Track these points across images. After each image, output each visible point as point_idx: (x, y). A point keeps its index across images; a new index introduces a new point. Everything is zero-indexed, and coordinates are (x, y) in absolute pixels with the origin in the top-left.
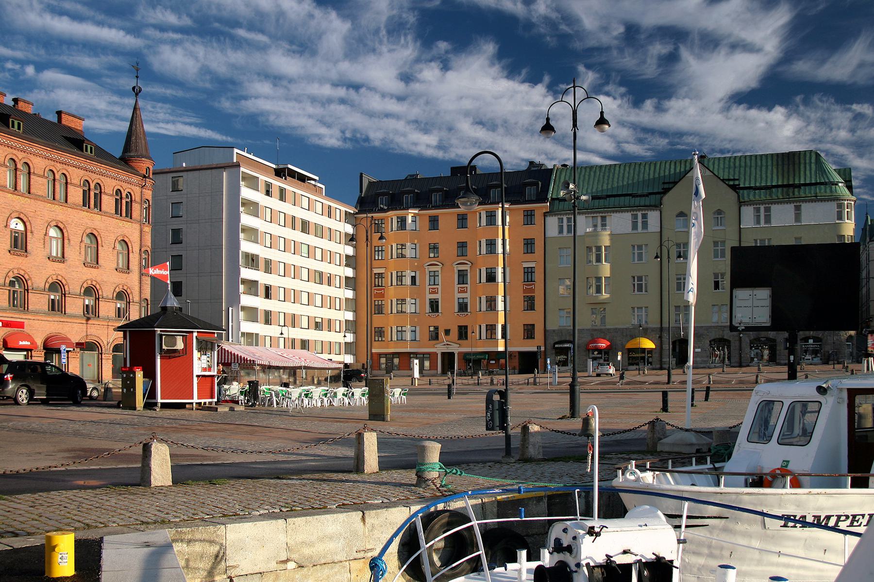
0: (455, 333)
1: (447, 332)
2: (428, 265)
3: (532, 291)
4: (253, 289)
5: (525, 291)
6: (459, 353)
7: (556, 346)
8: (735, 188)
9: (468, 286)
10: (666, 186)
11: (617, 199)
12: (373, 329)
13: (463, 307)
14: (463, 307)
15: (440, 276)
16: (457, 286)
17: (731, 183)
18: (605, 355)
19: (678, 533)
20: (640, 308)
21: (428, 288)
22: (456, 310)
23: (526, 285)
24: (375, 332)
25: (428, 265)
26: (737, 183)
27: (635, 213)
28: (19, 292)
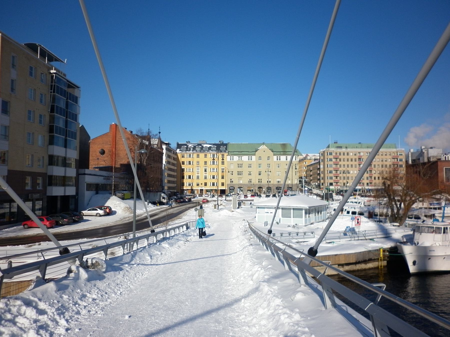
0: (203, 184)
1: (202, 184)
5: (222, 174)
6: (205, 189)
8: (272, 151)
9: (207, 172)
10: (256, 150)
13: (206, 178)
14: (206, 178)
16: (204, 172)
17: (272, 150)
20: (240, 172)
26: (273, 150)
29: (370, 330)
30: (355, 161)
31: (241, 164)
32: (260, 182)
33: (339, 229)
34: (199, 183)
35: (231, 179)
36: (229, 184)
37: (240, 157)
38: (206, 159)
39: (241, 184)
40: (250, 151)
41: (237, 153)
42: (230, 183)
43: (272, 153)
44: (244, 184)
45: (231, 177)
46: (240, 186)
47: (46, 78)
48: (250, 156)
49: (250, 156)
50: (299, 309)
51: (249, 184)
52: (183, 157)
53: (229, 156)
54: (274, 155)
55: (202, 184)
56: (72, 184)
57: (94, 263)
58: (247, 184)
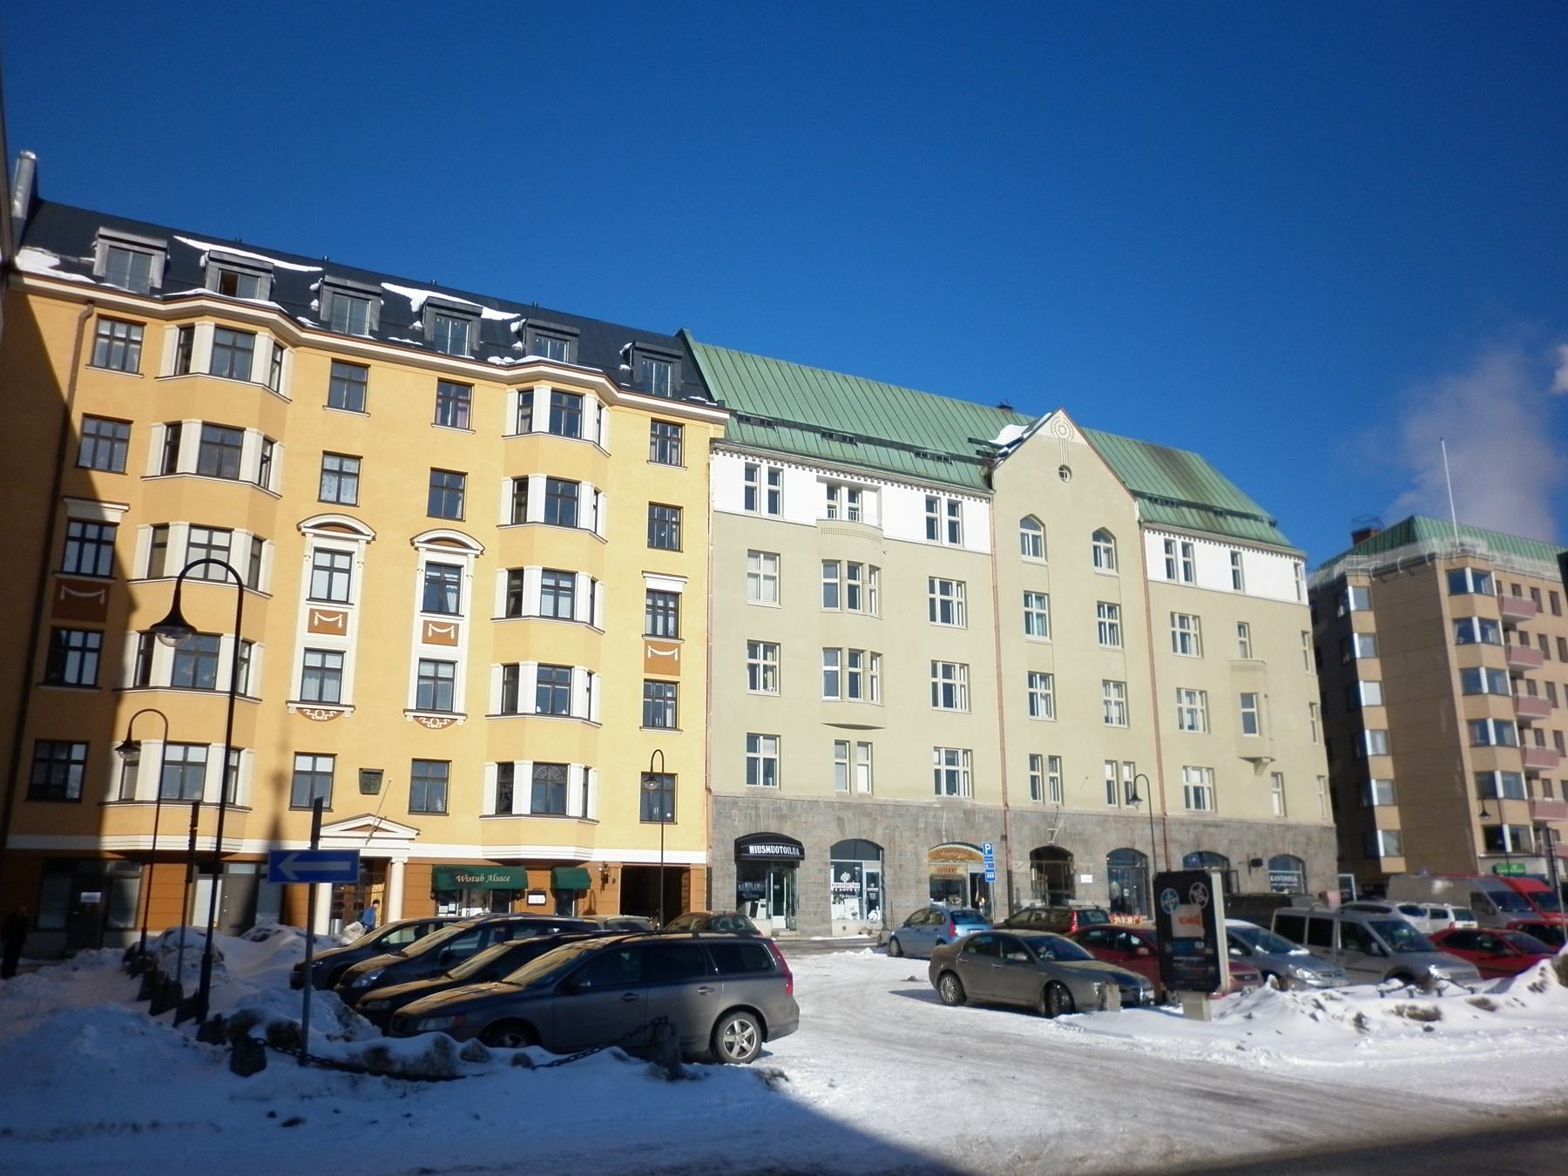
0: (397, 785)
1: (370, 780)
2: (429, 541)
3: (674, 667)
4: (136, 746)
5: (650, 664)
6: (411, 865)
7: (753, 849)
9: (464, 624)
11: (797, 433)
12: (28, 747)
15: (357, 572)
16: (419, 618)
18: (868, 886)
19: (312, 1063)
21: (304, 609)
22: (412, 705)
23: (654, 645)
24: (36, 760)
25: (429, 541)
27: (935, 494)
28: (1030, 536)
29: (768, 423)
30: (1479, 725)
31: (844, 570)
32: (1046, 787)
33: (1426, 1091)
34: (324, 765)
35: (752, 741)
36: (734, 801)
37: (844, 492)
38: (450, 449)
39: (862, 809)
40: (931, 448)
41: (811, 441)
42: (734, 783)
43: (1135, 508)
44: (900, 809)
45: (760, 712)
46: (851, 835)
47: (712, 577)
48: (944, 499)
49: (944, 499)
50: (1138, 937)
51: (945, 806)
52: (120, 357)
53: (737, 464)
54: (1146, 524)
55: (370, 780)
56: (919, 826)
57: (955, 929)
58: (925, 809)
